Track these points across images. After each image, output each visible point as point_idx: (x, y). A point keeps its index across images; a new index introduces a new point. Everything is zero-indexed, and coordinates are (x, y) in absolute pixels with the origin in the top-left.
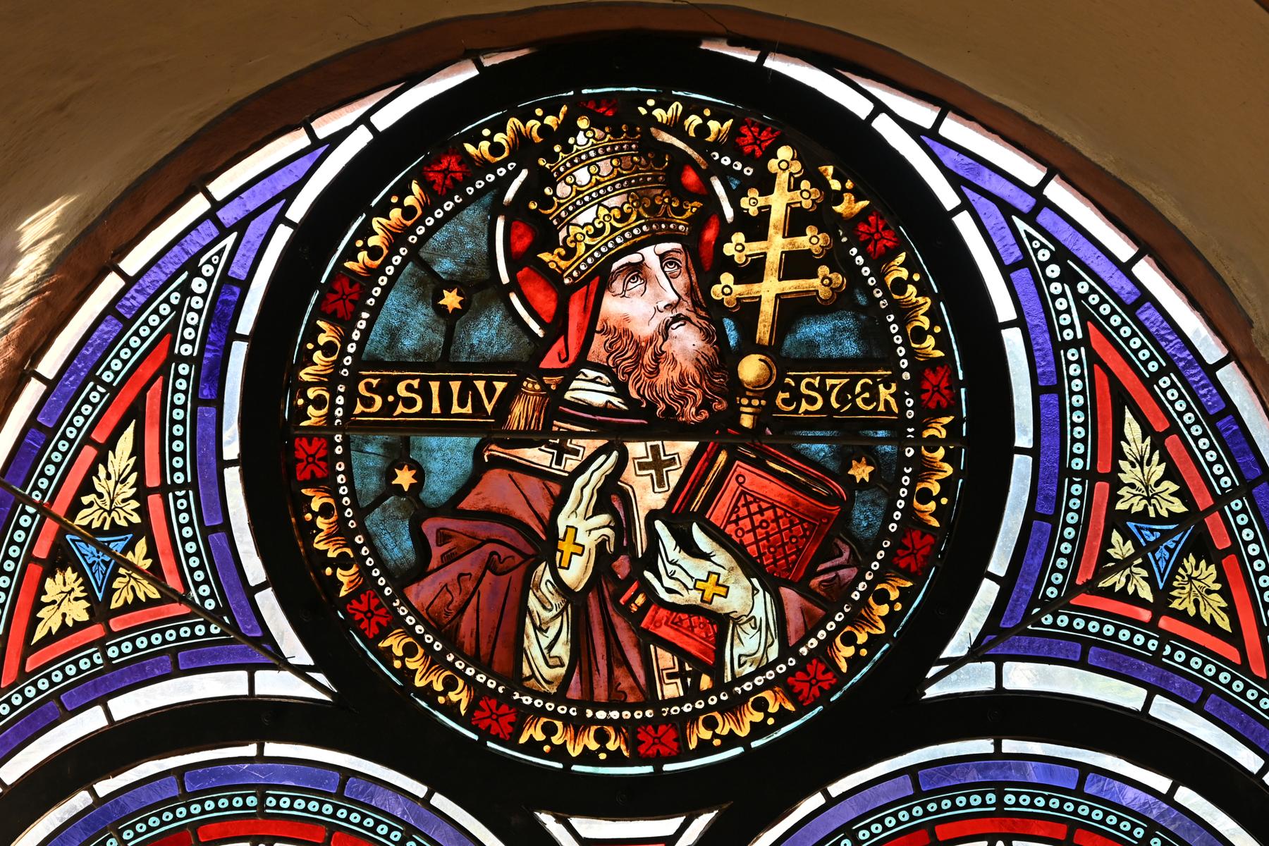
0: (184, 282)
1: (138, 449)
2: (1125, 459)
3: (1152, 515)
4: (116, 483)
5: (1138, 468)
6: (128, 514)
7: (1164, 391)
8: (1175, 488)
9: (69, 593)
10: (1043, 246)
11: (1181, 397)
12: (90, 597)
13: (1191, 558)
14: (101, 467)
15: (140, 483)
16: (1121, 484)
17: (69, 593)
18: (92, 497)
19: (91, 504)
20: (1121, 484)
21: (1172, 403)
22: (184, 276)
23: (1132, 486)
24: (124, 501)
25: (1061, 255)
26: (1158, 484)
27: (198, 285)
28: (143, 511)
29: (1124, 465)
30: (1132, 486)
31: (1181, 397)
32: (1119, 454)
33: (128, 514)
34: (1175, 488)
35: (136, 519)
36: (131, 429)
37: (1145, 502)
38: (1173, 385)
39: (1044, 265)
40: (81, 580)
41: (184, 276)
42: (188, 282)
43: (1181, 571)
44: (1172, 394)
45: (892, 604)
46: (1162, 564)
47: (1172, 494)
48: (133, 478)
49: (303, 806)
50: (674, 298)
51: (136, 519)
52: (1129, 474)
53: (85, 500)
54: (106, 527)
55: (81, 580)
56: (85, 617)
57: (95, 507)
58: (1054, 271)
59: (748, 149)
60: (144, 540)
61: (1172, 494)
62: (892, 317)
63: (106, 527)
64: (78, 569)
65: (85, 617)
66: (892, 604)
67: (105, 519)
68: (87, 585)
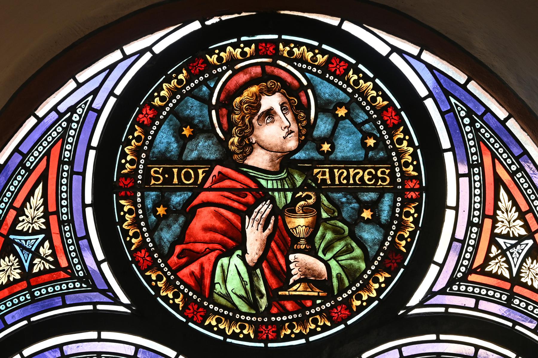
0: (69, 117)
1: (45, 195)
2: (500, 209)
3: (511, 236)
4: (34, 210)
5: (505, 213)
6: (40, 224)
7: (519, 179)
8: (522, 223)
9: (11, 266)
10: (462, 109)
11: (526, 182)
12: (22, 267)
13: (530, 258)
14: (28, 204)
15: (46, 211)
16: (497, 221)
17: (11, 266)
18: (24, 217)
19: (23, 220)
20: (497, 221)
21: (522, 184)
22: (69, 114)
23: (503, 222)
24: (38, 218)
25: (470, 113)
26: (514, 221)
27: (76, 117)
28: (47, 223)
29: (498, 212)
30: (503, 222)
31: (526, 182)
32: (497, 207)
33: (40, 224)
34: (522, 223)
35: (44, 227)
36: (41, 186)
37: (508, 229)
38: (523, 177)
39: (462, 118)
40: (17, 260)
41: (69, 114)
42: (71, 116)
43: (524, 264)
44: (522, 180)
45: (218, 54)
46: (515, 260)
47: (520, 226)
48: (42, 209)
49: (42, 148)
50: (288, 124)
51: (44, 227)
52: (500, 216)
53: (21, 219)
54: (30, 232)
55: (17, 260)
56: (18, 277)
57: (25, 221)
58: (467, 121)
59: (386, 118)
60: (47, 241)
61: (520, 226)
62: (328, 75)
63: (30, 232)
64: (17, 255)
65: (18, 277)
66: (218, 54)
67: (30, 227)
68: (20, 262)
